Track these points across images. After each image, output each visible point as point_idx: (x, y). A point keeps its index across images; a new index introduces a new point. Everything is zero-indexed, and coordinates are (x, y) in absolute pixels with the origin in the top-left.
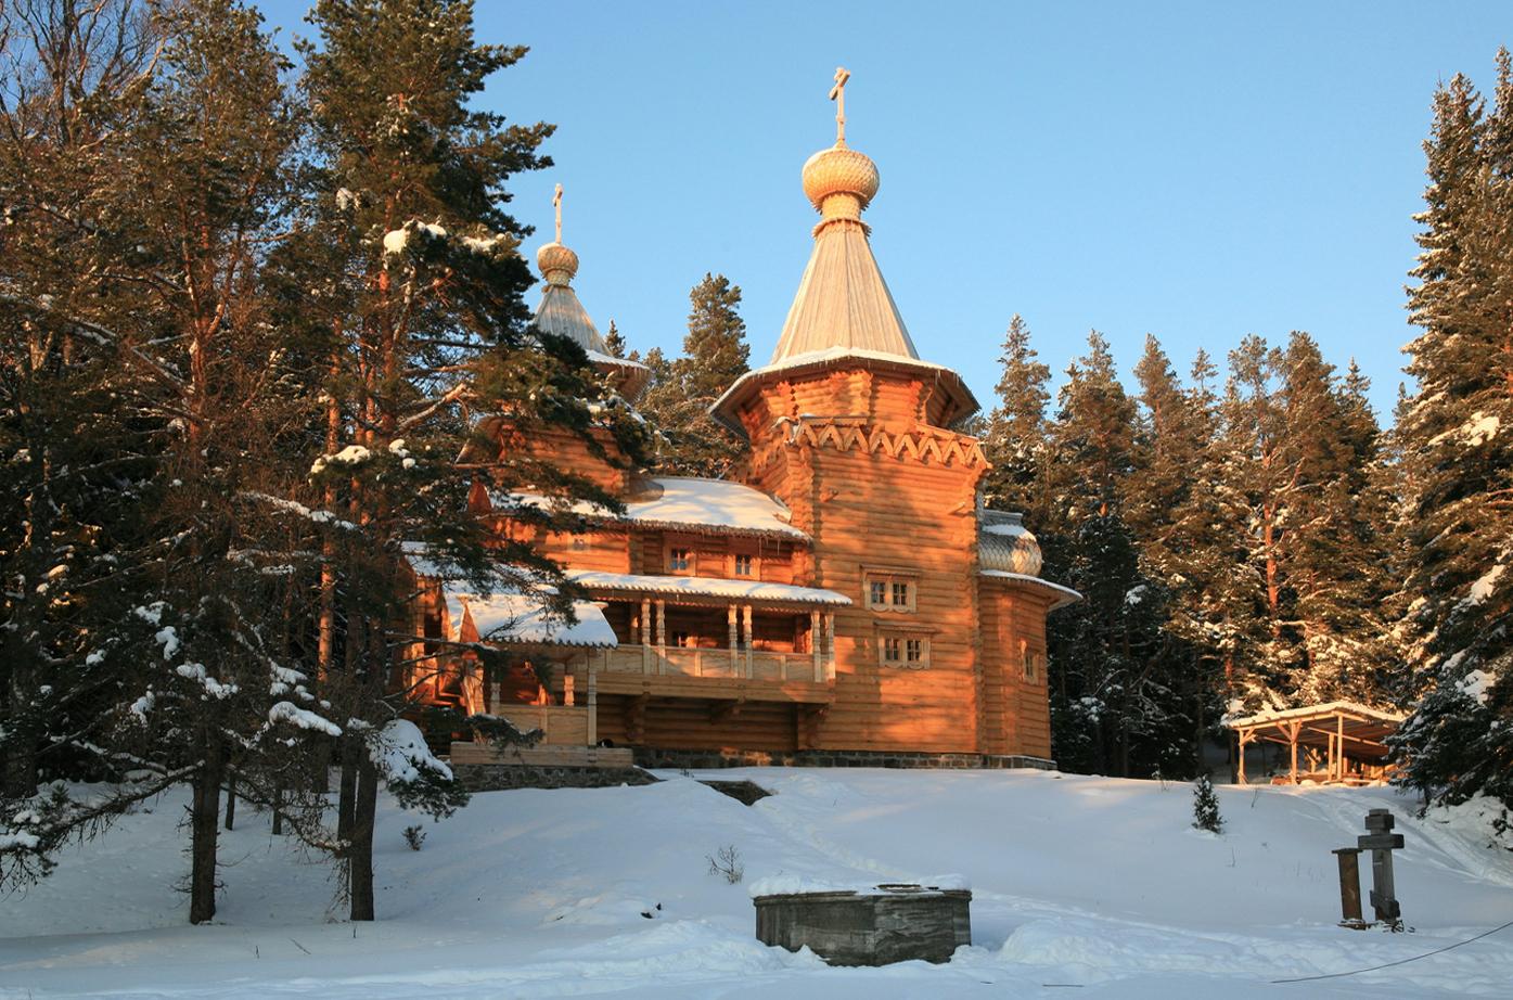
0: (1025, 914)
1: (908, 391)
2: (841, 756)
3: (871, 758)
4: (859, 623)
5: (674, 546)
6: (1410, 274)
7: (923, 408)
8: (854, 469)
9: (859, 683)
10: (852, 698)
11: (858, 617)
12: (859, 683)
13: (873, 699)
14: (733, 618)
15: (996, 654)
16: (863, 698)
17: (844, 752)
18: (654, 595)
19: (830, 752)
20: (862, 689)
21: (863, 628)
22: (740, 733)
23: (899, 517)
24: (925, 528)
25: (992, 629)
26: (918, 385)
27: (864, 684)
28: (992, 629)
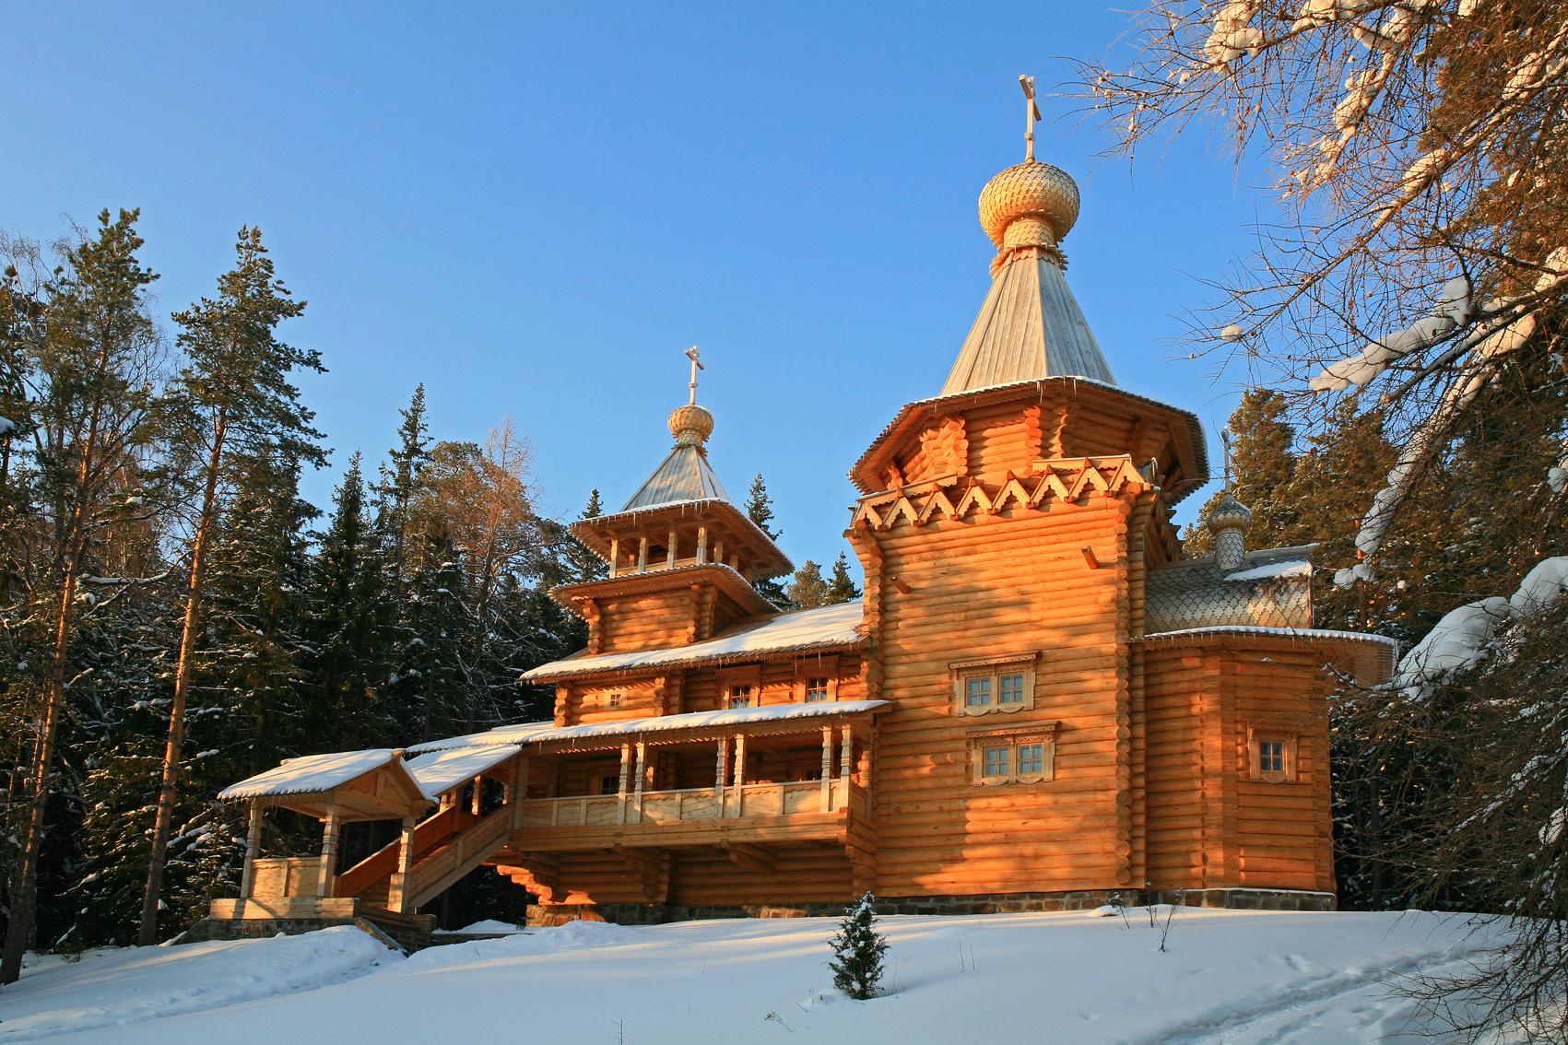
0: (292, 892)
1: (1024, 426)
2: (908, 903)
3: (954, 903)
4: (946, 734)
5: (736, 683)
6: (595, 493)
7: (1056, 440)
8: (914, 557)
9: (941, 810)
10: (929, 830)
11: (946, 728)
12: (941, 810)
13: (958, 829)
14: (625, 754)
15: (1187, 747)
16: (944, 829)
17: (912, 898)
18: (729, 730)
19: (892, 899)
20: (946, 817)
21: (952, 740)
22: (800, 883)
23: (1013, 581)
24: (1013, 598)
25: (1182, 712)
26: (1033, 414)
27: (950, 811)
28: (1182, 712)
